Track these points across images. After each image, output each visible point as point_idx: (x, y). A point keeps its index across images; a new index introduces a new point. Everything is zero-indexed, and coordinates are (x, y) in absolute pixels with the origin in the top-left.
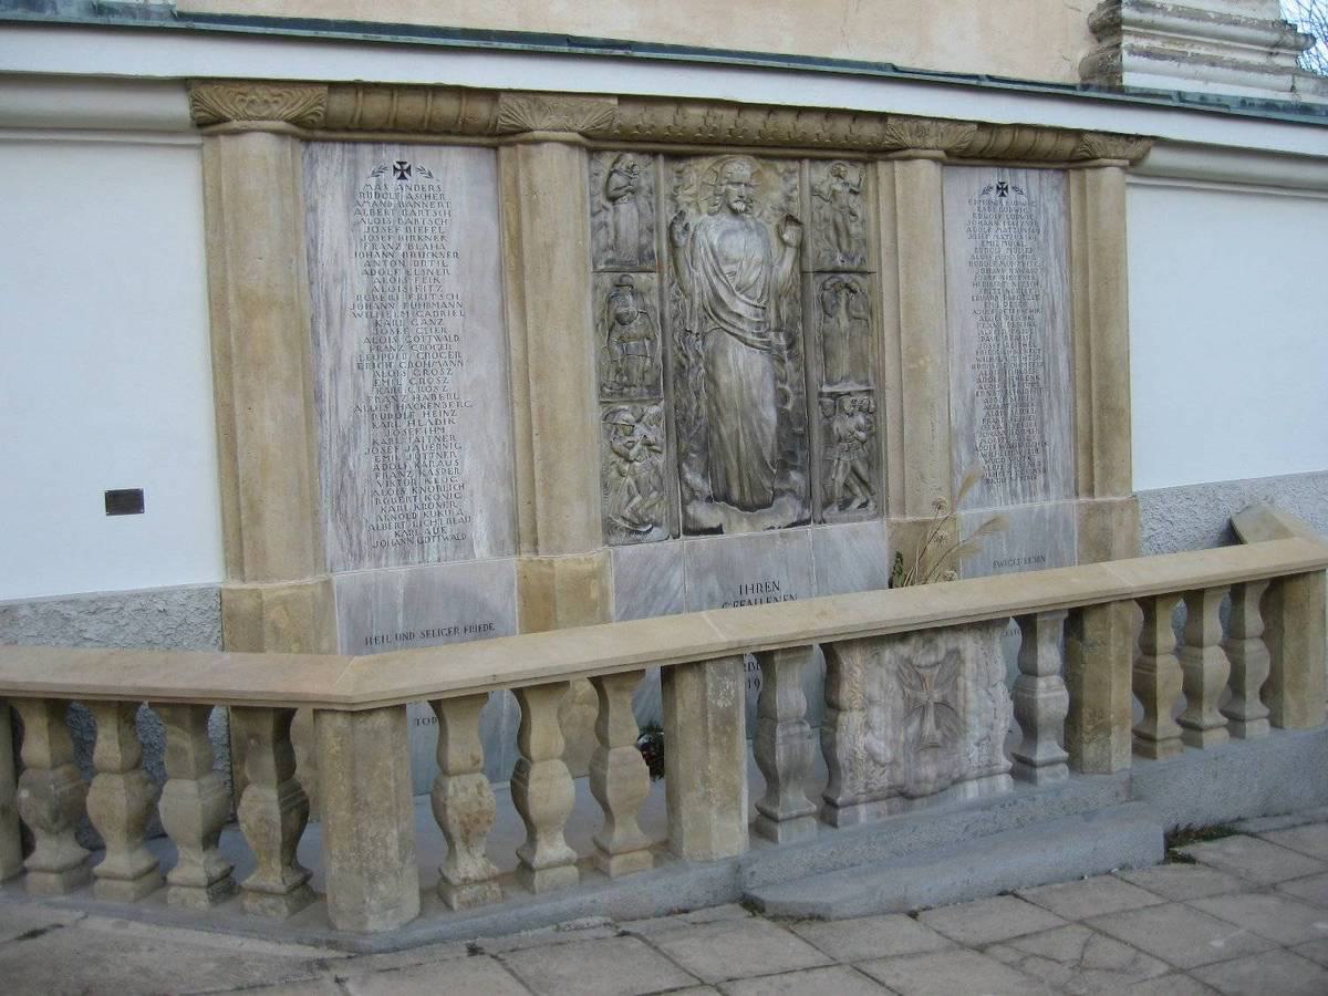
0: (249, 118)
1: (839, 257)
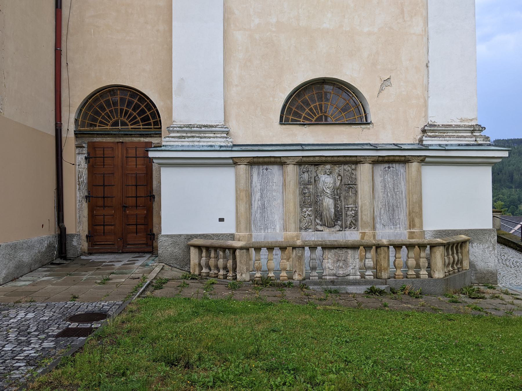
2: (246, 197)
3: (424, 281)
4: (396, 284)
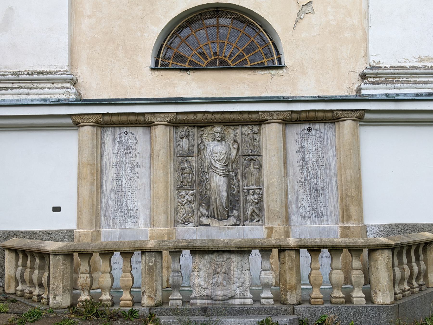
0: (85, 122)
1: (250, 151)
2: (92, 174)
3: (357, 309)
4: (311, 314)
